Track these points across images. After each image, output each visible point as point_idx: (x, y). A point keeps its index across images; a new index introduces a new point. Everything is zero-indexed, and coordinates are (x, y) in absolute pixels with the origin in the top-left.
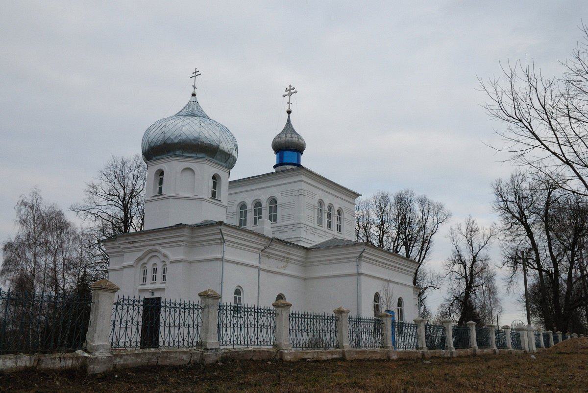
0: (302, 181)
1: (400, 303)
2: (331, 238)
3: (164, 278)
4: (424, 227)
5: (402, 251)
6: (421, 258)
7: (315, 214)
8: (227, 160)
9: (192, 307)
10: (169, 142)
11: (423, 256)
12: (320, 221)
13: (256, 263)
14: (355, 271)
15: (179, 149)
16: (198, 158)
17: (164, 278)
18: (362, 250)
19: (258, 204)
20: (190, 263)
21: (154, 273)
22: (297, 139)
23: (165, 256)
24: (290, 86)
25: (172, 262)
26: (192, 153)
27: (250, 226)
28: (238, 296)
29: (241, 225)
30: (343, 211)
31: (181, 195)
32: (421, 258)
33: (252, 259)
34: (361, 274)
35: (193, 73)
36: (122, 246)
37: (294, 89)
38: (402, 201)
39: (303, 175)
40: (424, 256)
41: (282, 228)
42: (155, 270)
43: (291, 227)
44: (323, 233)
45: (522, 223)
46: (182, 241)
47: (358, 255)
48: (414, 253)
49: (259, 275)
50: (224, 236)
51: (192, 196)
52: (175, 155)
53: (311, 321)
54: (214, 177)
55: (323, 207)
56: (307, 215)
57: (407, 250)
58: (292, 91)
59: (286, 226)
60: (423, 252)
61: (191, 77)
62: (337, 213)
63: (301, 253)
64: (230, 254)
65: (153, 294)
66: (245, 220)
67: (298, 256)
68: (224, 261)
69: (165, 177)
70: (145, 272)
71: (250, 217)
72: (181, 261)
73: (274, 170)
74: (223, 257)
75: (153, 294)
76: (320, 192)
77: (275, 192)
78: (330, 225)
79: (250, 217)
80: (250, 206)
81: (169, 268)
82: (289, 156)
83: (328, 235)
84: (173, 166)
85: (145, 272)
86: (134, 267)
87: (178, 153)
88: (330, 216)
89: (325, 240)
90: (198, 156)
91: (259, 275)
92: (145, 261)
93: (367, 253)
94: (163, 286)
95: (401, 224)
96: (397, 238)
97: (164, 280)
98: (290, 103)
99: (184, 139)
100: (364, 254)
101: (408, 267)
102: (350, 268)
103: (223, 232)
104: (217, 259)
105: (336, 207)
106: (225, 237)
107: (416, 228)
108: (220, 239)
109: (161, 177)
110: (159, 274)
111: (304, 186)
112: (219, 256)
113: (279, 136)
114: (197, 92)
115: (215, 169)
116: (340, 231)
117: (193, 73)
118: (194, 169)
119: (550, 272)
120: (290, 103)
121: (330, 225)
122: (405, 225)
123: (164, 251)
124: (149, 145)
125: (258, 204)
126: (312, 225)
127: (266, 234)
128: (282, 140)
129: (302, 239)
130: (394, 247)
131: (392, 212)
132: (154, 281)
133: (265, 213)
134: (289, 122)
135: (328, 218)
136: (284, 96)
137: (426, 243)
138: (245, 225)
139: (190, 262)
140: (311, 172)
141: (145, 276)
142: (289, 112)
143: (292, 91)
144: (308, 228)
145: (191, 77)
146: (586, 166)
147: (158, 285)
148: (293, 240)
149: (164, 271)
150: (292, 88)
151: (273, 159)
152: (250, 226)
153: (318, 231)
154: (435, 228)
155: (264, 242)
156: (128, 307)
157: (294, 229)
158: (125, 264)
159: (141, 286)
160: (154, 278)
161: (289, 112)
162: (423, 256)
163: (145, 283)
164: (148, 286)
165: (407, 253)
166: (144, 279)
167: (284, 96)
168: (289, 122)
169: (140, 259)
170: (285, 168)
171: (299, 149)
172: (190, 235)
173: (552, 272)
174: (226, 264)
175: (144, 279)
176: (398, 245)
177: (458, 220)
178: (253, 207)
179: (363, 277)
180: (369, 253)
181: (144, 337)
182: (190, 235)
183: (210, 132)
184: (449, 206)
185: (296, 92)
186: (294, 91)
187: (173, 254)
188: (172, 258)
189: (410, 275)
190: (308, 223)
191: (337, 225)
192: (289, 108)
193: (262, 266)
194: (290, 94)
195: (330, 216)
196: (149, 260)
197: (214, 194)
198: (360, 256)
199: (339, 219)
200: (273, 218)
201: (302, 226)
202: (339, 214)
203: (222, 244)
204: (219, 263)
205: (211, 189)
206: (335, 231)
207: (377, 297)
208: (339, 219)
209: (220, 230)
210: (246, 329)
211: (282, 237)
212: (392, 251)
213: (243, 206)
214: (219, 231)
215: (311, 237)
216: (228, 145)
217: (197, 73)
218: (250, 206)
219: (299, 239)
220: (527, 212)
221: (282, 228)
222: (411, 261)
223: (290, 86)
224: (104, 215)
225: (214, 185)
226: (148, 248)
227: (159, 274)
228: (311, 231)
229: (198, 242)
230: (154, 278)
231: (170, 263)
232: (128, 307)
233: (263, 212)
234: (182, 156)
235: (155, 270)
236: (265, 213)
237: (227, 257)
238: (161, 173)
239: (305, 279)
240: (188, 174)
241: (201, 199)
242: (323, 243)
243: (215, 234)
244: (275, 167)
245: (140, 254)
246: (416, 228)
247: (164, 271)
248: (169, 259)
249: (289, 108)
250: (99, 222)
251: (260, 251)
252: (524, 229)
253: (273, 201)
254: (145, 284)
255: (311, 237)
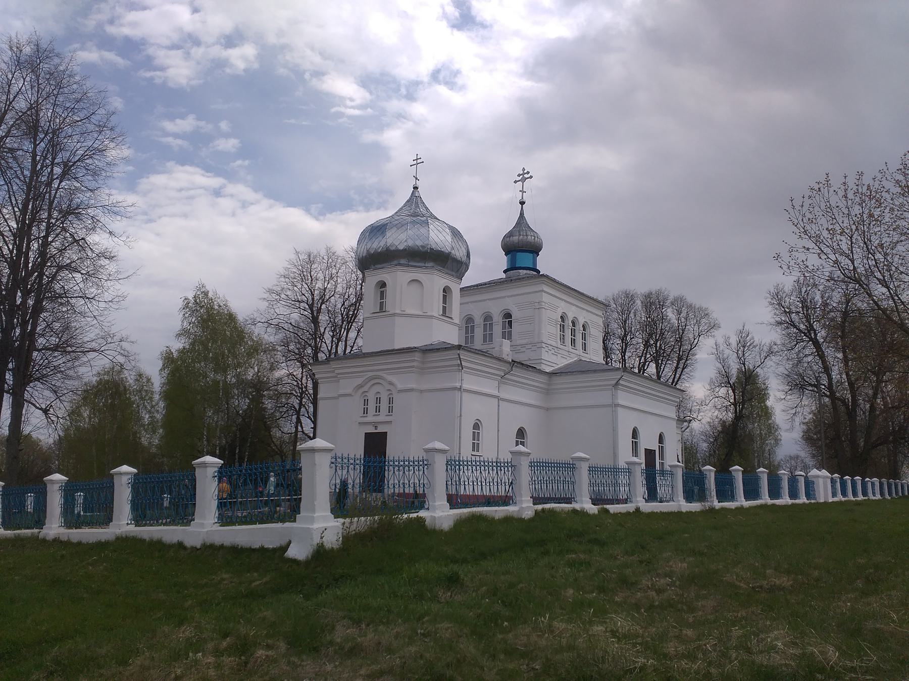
0: (543, 291)
1: (661, 439)
2: (576, 359)
3: (390, 410)
4: (680, 340)
5: (652, 369)
6: (676, 380)
7: (556, 331)
8: (459, 269)
9: (506, 464)
10: (393, 248)
11: (678, 375)
12: (563, 338)
13: (495, 393)
14: (609, 402)
15: (404, 258)
16: (427, 267)
17: (390, 410)
18: (619, 377)
19: (488, 318)
20: (421, 392)
21: (390, 404)
22: (533, 237)
23: (391, 383)
24: (524, 169)
25: (400, 391)
26: (419, 262)
27: (478, 344)
28: (476, 431)
29: (466, 343)
30: (588, 325)
31: (408, 311)
32: (676, 380)
33: (489, 386)
34: (618, 405)
35: (414, 160)
36: (337, 371)
37: (528, 173)
38: (654, 303)
39: (543, 283)
40: (680, 376)
41: (519, 348)
42: (378, 400)
43: (529, 346)
44: (566, 353)
45: (811, 339)
46: (413, 367)
47: (614, 382)
48: (668, 372)
49: (499, 406)
50: (462, 362)
51: (421, 313)
52: (400, 264)
53: (501, 470)
54: (444, 291)
55: (566, 321)
56: (550, 332)
57: (658, 367)
58: (526, 176)
59: (523, 345)
60: (679, 370)
61: (411, 166)
62: (582, 329)
63: (543, 379)
64: (470, 382)
65: (376, 428)
66: (473, 337)
67: (541, 382)
68: (462, 390)
69: (389, 289)
70: (366, 402)
71: (479, 333)
72: (411, 390)
73: (504, 276)
74: (461, 386)
75: (376, 428)
76: (563, 304)
77: (511, 305)
78: (573, 342)
79: (479, 333)
80: (479, 321)
81: (397, 398)
82: (524, 259)
83: (572, 355)
84: (387, 275)
85: (366, 402)
86: (352, 396)
87: (403, 261)
88: (573, 333)
89: (569, 362)
90: (426, 265)
91: (499, 406)
92: (365, 388)
93: (626, 381)
94: (388, 419)
95: (650, 335)
96: (644, 354)
97: (376, 412)
98: (523, 192)
99: (410, 245)
100: (621, 382)
101: (654, 390)
102: (604, 397)
103: (461, 357)
104: (455, 389)
105: (581, 321)
106: (463, 363)
107: (671, 339)
108: (458, 365)
109: (382, 289)
110: (384, 406)
111: (546, 298)
112: (458, 385)
113: (510, 234)
114: (419, 184)
115: (411, 274)
116: (585, 350)
117: (414, 160)
118: (423, 283)
119: (847, 401)
120: (523, 192)
121: (573, 342)
122: (656, 337)
123: (390, 378)
124: (368, 251)
125: (488, 318)
126: (554, 344)
127: (505, 357)
128: (515, 239)
129: (543, 361)
130: (640, 363)
131: (639, 315)
132: (378, 413)
133: (498, 330)
134: (522, 214)
135: (582, 339)
136: (516, 182)
137: (684, 360)
138: (472, 342)
139: (421, 391)
140: (554, 280)
141: (366, 407)
142: (522, 203)
143: (526, 176)
144: (550, 348)
145: (411, 166)
146: (908, 251)
147: (382, 418)
148: (531, 362)
149: (391, 401)
150: (525, 172)
151: (503, 261)
152: (478, 344)
153: (560, 351)
154: (696, 341)
155: (506, 368)
156: (414, 468)
157: (534, 348)
158: (342, 392)
159: (362, 419)
160: (378, 409)
161: (522, 203)
162: (678, 375)
163: (391, 414)
164: (370, 418)
165: (658, 372)
166: (366, 411)
167: (516, 182)
168: (522, 214)
169: (360, 386)
170: (519, 273)
171: (535, 250)
172: (548, 382)
173: (849, 401)
174: (465, 395)
175: (366, 411)
176: (646, 361)
177: (727, 332)
178: (482, 320)
179: (620, 410)
180: (628, 380)
181: (382, 476)
182: (548, 382)
183: (440, 236)
184: (717, 311)
185: (531, 177)
186: (529, 176)
187: (400, 381)
188: (400, 386)
189: (673, 405)
190: (550, 342)
191: (572, 338)
192: (522, 198)
193: (503, 395)
194: (524, 180)
195: (573, 333)
196: (370, 388)
197: (444, 308)
198: (617, 384)
199: (584, 337)
200: (507, 335)
201: (544, 345)
202: (584, 330)
203: (459, 372)
204: (458, 393)
205: (441, 304)
206: (568, 347)
207: (635, 433)
208: (584, 337)
209: (459, 354)
210: (551, 485)
211: (519, 358)
212: (636, 371)
213: (469, 320)
214: (458, 356)
215: (553, 359)
216: (460, 251)
217: (419, 161)
218: (479, 321)
219: (539, 361)
220: (816, 326)
221: (519, 348)
222: (646, 378)
223: (524, 169)
224: (286, 326)
225: (445, 297)
226: (370, 374)
227: (384, 406)
228: (553, 351)
229: (429, 368)
230: (378, 409)
231: (398, 392)
232: (414, 468)
233: (495, 327)
234: (408, 266)
235: (378, 400)
236: (498, 330)
237: (466, 386)
238: (383, 285)
239: (547, 409)
240: (415, 286)
241: (431, 317)
242: (567, 365)
243: (451, 359)
244: (505, 272)
245: (360, 381)
246: (671, 339)
247: (391, 401)
248: (396, 388)
249: (522, 198)
250: (280, 336)
251: (500, 378)
252: (812, 347)
253: (508, 315)
254: (367, 416)
255: (553, 359)
